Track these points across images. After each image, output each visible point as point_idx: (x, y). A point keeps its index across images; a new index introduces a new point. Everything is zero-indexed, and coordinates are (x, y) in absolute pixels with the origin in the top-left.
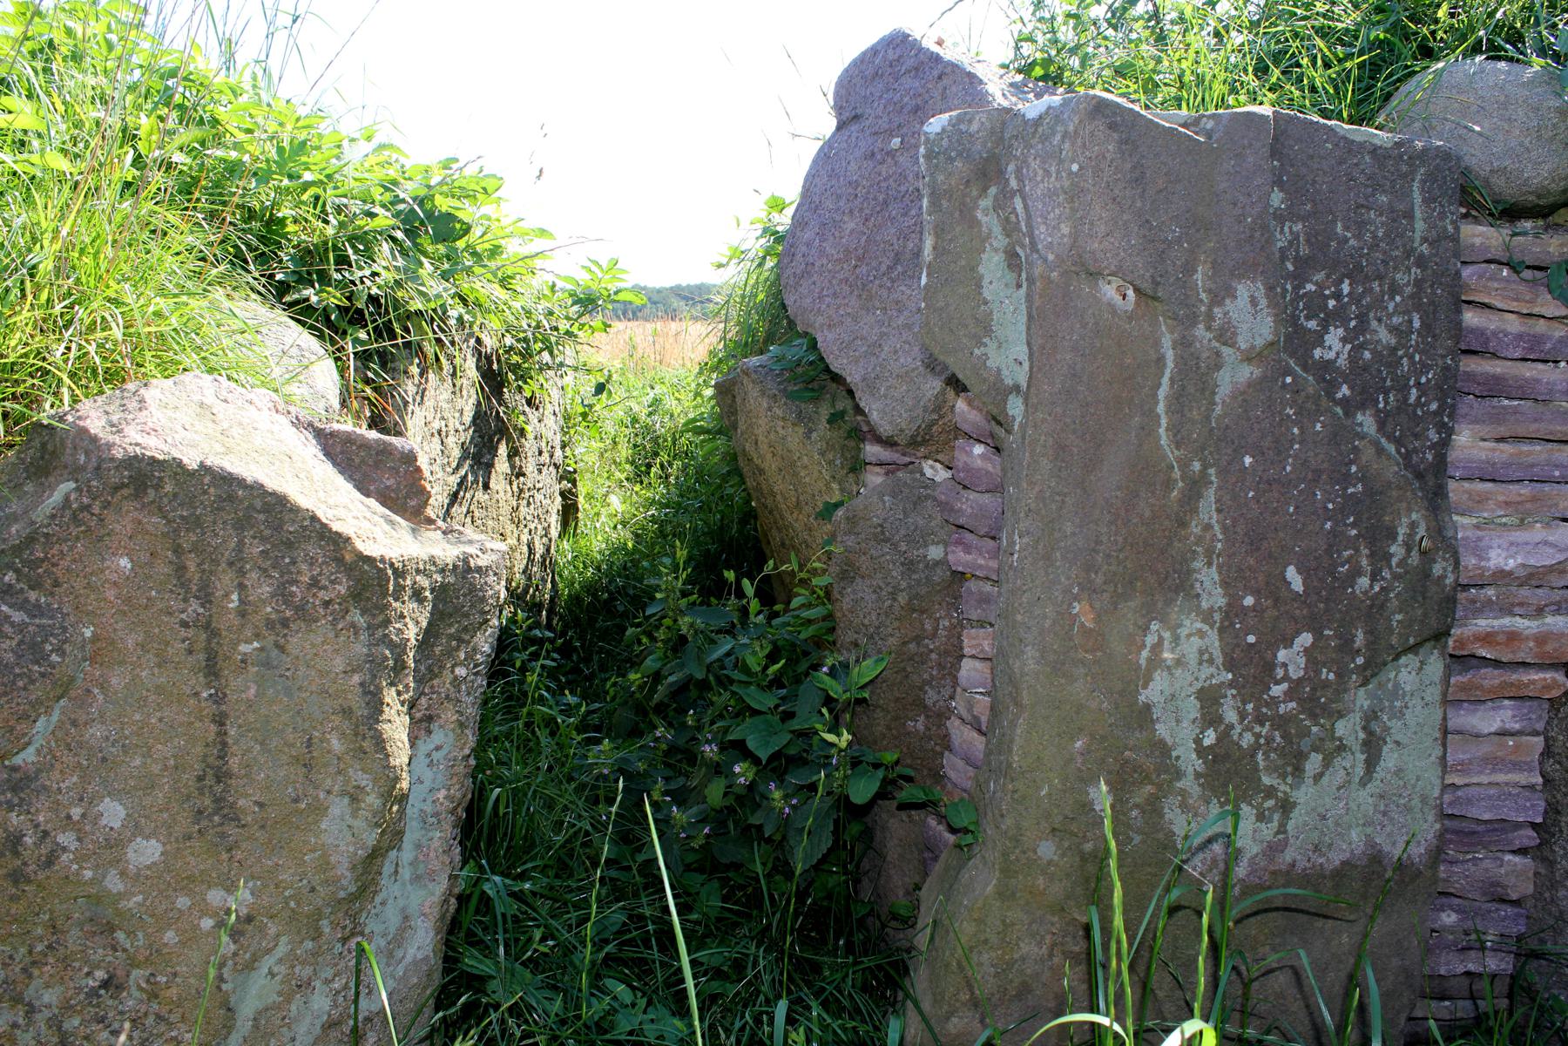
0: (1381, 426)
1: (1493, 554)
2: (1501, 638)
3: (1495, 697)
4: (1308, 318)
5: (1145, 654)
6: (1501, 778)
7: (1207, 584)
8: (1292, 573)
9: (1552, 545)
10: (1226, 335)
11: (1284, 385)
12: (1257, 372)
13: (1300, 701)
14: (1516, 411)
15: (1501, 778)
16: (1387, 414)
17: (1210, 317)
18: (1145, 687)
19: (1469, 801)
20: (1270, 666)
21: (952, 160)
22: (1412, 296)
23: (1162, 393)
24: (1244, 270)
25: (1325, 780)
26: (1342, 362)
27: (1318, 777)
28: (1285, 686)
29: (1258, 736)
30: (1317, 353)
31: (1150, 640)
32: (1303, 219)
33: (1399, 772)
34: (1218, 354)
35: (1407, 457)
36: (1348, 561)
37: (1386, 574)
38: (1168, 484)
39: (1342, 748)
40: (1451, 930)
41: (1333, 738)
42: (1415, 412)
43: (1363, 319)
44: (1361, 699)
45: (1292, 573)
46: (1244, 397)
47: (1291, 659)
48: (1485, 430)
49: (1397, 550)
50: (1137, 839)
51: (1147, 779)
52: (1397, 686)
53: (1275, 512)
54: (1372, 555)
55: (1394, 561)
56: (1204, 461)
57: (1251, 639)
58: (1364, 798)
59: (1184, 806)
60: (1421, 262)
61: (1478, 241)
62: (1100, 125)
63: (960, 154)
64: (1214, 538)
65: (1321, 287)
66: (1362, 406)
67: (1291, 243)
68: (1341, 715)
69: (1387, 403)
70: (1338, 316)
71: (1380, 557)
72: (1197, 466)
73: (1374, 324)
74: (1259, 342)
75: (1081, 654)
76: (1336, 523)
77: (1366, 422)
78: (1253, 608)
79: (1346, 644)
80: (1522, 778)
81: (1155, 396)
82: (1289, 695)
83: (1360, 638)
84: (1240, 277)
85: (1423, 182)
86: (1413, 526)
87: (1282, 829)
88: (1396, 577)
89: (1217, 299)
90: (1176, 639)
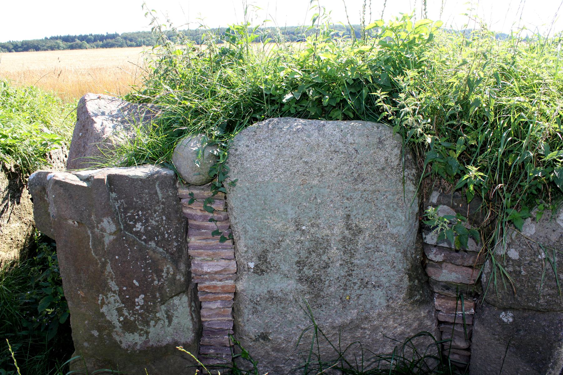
0: (157, 244)
1: (204, 268)
2: (212, 287)
3: (215, 300)
4: (130, 221)
5: (99, 301)
6: (220, 318)
7: (113, 285)
8: (135, 281)
9: (220, 266)
10: (103, 230)
11: (123, 240)
12: (115, 237)
13: (144, 310)
14: (206, 233)
15: (220, 318)
16: (158, 241)
17: (98, 227)
18: (101, 308)
19: (213, 324)
20: (134, 303)
21: (36, 186)
22: (162, 212)
23: (90, 243)
24: (104, 215)
25: (157, 326)
26: (142, 231)
27: (154, 326)
28: (139, 307)
29: (135, 318)
30: (134, 229)
31: (100, 298)
32: (123, 199)
33: (178, 323)
34: (102, 234)
35: (167, 251)
36: (151, 277)
37: (162, 280)
38: (97, 264)
39: (159, 319)
40: (213, 353)
41: (156, 317)
42: (168, 239)
43: (147, 220)
44: (163, 307)
45: (135, 281)
46: (112, 243)
47: (140, 300)
48: (198, 237)
49: (164, 275)
50: (108, 342)
51: (106, 329)
52: (174, 304)
53: (127, 268)
54: (157, 276)
55: (164, 277)
56: (105, 258)
57: (127, 297)
58: (170, 329)
59: (117, 334)
60: (163, 203)
61: (184, 194)
62: (57, 186)
63: (38, 184)
64: (112, 275)
65: (132, 213)
66: (150, 240)
67: (121, 205)
68: (157, 312)
69: (158, 239)
70: (139, 220)
71: (160, 277)
72: (103, 259)
73: (151, 220)
74: (112, 231)
75: (82, 302)
76: (145, 269)
77: (152, 244)
78: (126, 290)
79: (154, 297)
80: (226, 318)
81: (89, 244)
82: (141, 309)
83: (158, 295)
84: (104, 217)
85: (159, 185)
86: (168, 268)
87: (147, 337)
88: (165, 280)
89: (99, 223)
90: (107, 298)
